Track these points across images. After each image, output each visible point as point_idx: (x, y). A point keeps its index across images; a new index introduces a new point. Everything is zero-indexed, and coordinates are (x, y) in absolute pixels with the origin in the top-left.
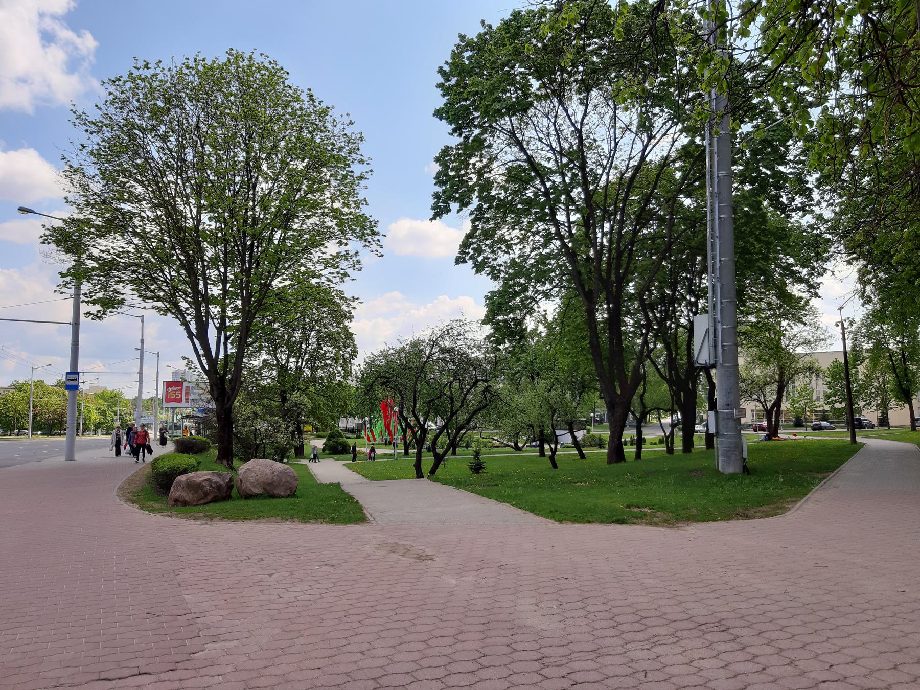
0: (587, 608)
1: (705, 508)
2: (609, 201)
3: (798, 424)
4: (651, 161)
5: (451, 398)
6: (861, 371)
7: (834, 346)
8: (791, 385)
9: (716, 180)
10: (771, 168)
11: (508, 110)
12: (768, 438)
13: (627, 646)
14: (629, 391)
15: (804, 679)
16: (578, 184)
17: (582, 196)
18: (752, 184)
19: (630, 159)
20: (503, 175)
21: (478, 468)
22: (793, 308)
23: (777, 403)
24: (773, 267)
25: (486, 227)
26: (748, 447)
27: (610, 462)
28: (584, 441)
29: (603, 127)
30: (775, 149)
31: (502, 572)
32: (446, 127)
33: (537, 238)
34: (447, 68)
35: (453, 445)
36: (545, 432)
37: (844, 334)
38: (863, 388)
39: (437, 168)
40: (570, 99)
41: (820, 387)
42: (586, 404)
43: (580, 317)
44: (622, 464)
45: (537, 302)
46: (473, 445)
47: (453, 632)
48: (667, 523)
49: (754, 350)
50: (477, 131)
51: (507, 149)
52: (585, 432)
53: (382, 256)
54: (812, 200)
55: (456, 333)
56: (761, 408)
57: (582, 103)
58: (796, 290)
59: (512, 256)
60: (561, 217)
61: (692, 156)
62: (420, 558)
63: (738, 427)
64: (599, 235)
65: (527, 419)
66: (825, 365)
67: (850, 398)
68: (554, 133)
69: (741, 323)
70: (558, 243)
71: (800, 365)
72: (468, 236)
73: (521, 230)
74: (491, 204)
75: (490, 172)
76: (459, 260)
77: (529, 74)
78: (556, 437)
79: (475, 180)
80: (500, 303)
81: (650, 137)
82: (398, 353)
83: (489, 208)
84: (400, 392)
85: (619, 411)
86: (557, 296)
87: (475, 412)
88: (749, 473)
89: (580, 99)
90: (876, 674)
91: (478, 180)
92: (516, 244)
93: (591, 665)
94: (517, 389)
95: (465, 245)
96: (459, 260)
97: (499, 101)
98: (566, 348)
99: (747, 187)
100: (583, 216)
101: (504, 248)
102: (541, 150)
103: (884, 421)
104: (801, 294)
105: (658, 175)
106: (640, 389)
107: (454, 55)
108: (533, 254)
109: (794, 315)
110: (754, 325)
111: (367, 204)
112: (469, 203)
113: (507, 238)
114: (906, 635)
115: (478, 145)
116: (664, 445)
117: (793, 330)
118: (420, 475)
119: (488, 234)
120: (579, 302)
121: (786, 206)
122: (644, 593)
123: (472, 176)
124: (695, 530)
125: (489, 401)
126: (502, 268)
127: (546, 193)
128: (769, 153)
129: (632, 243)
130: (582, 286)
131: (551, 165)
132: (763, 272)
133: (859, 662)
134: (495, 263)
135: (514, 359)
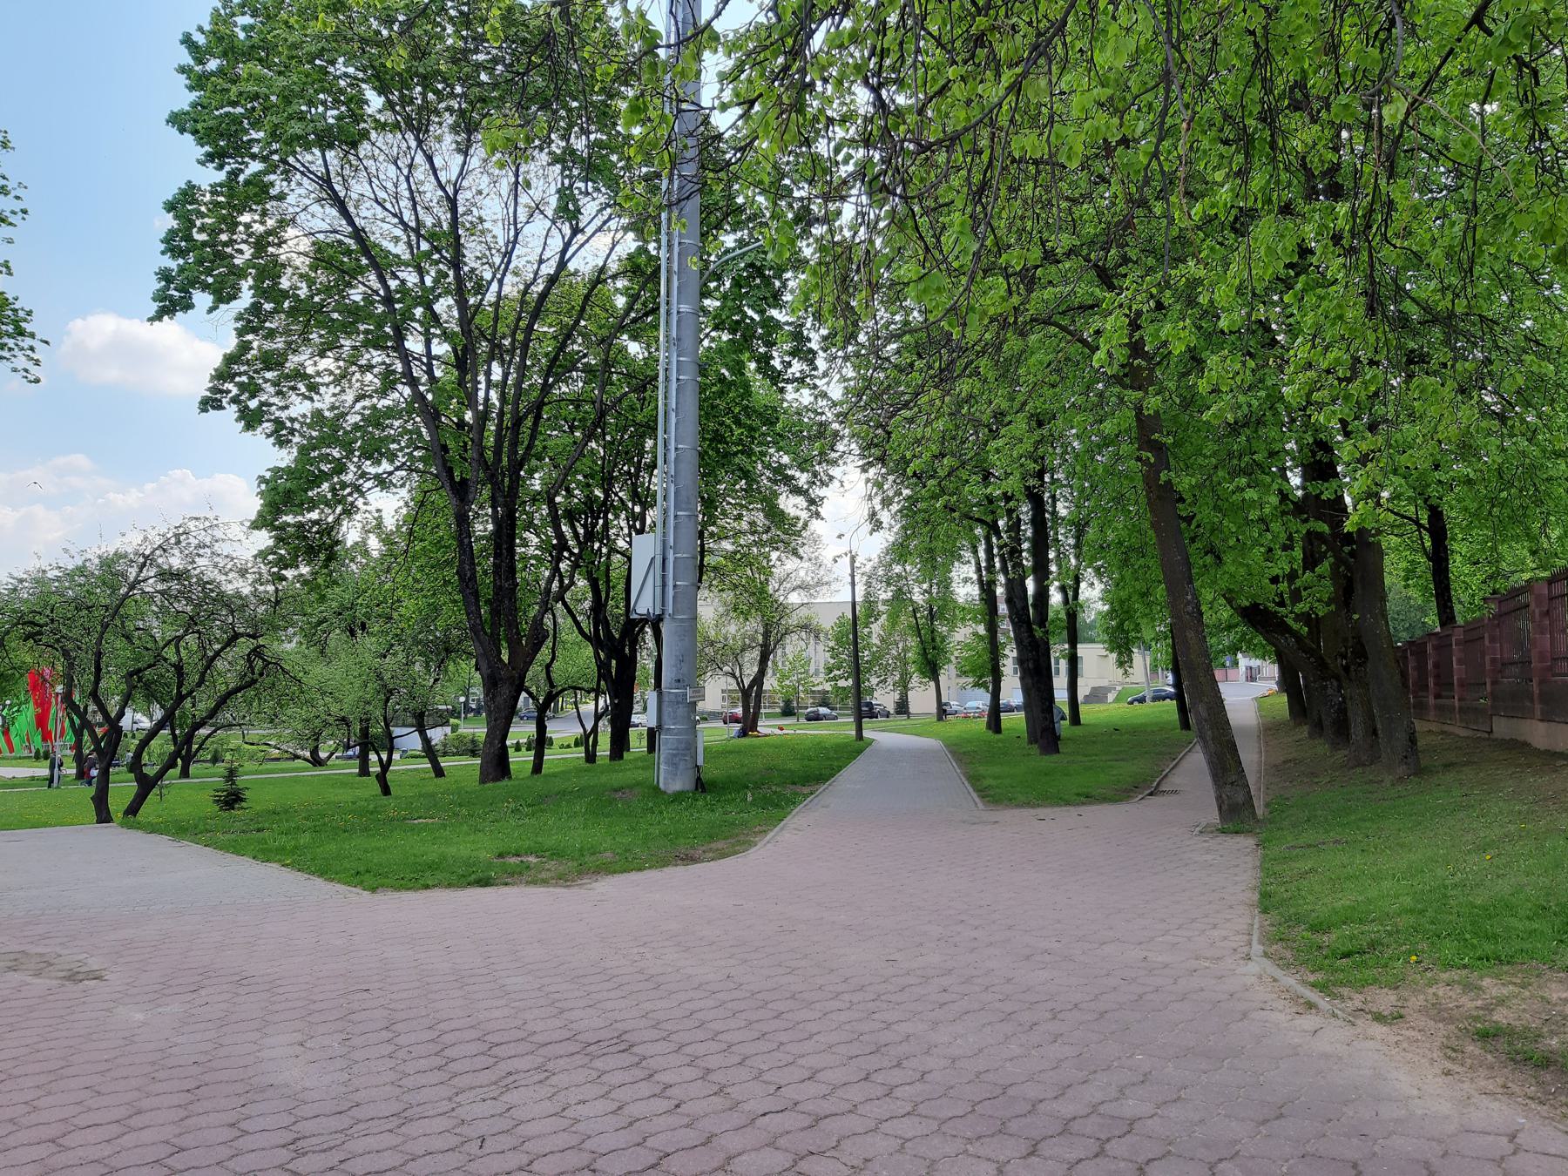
0: (396, 1040)
1: (627, 850)
2: (502, 329)
3: (788, 712)
4: (576, 272)
5: (179, 668)
6: (875, 631)
7: (838, 596)
8: (779, 652)
9: (675, 318)
10: (762, 312)
11: (320, 139)
12: (744, 733)
13: (457, 1099)
14: (524, 659)
15: (735, 1115)
16: (447, 292)
17: (456, 313)
18: (733, 331)
19: (541, 262)
20: (305, 254)
21: (232, 799)
22: (785, 533)
23: (758, 680)
24: (760, 467)
25: (268, 346)
26: (705, 749)
27: (483, 781)
28: (445, 745)
29: (497, 199)
30: (767, 281)
31: (241, 990)
32: (189, 148)
33: (369, 377)
34: (200, 39)
35: (184, 754)
36: (372, 731)
37: (853, 576)
38: (876, 658)
39: (170, 222)
40: (439, 139)
41: (819, 656)
42: (450, 680)
43: (445, 526)
44: (505, 782)
45: (362, 494)
46: (228, 756)
47: (122, 1112)
48: (563, 879)
49: (729, 596)
50: (255, 167)
51: (316, 208)
52: (448, 730)
53: (37, 381)
54: (815, 369)
55: (194, 542)
56: (734, 686)
57: (459, 151)
58: (791, 504)
59: (318, 405)
60: (414, 344)
61: (642, 270)
62: (73, 977)
63: (691, 714)
64: (482, 386)
65: (334, 709)
66: (827, 622)
67: (857, 672)
68: (407, 194)
69: (711, 552)
70: (407, 391)
71: (793, 621)
72: (230, 359)
73: (337, 360)
74: (279, 303)
75: (279, 245)
76: (210, 403)
77: (363, 81)
78: (392, 739)
79: (247, 255)
80: (289, 492)
81: (576, 231)
82: (70, 575)
83: (275, 311)
84: (66, 654)
85: (505, 691)
86: (403, 486)
87: (230, 694)
88: (704, 791)
89: (458, 143)
90: (839, 1093)
91: (254, 256)
92: (327, 385)
93: (391, 1140)
94: (322, 652)
95: (223, 374)
96: (210, 403)
97: (300, 119)
98: (416, 581)
99: (725, 337)
100: (455, 350)
101: (303, 390)
102: (383, 221)
103: (902, 707)
104: (799, 513)
105: (587, 297)
106: (544, 654)
107: (216, 17)
108: (358, 406)
109: (787, 544)
110: (730, 556)
111: (10, 274)
112: (235, 297)
113: (310, 370)
114: (888, 1026)
115: (259, 192)
116: (582, 749)
117: (784, 566)
118: (104, 816)
119: (271, 361)
120: (442, 499)
121: (779, 373)
122: (503, 1002)
123: (244, 247)
124: (607, 886)
125: (261, 672)
126: (297, 426)
127: (388, 300)
128: (758, 287)
129: (538, 407)
130: (450, 471)
131: (400, 250)
132: (746, 474)
133: (819, 1076)
134: (283, 415)
135: (314, 596)
